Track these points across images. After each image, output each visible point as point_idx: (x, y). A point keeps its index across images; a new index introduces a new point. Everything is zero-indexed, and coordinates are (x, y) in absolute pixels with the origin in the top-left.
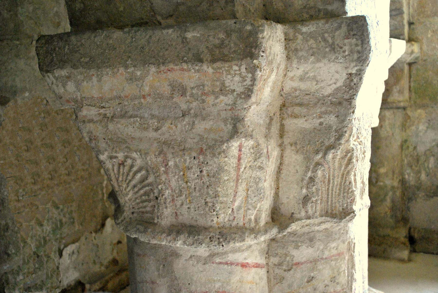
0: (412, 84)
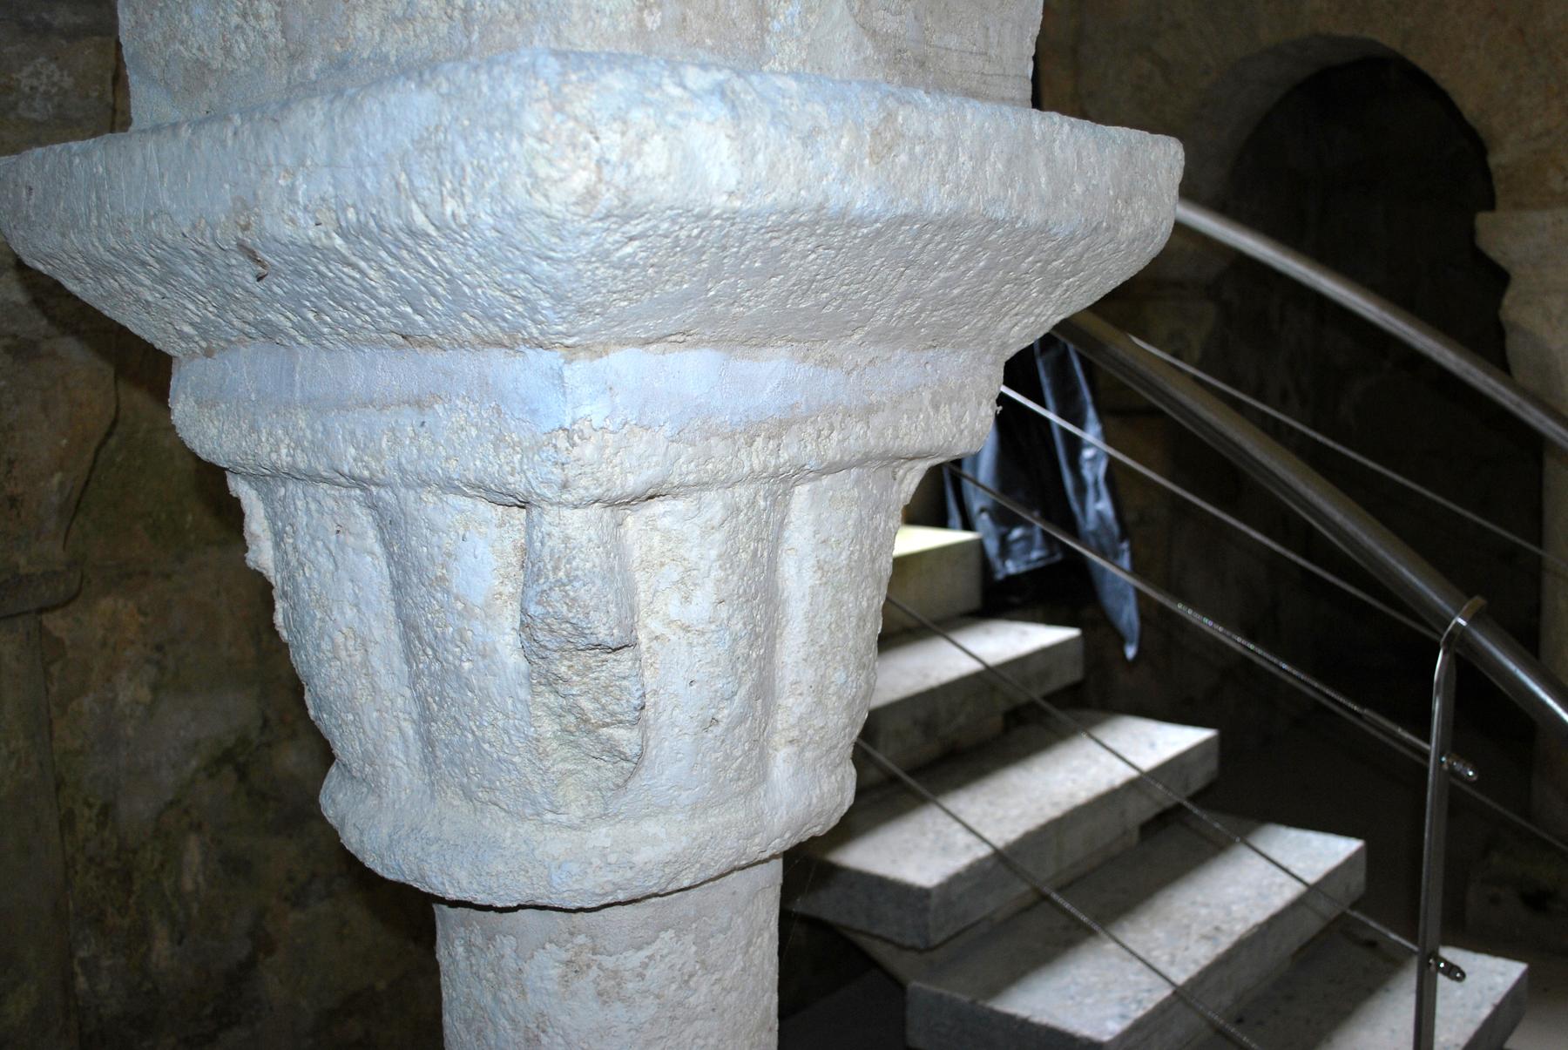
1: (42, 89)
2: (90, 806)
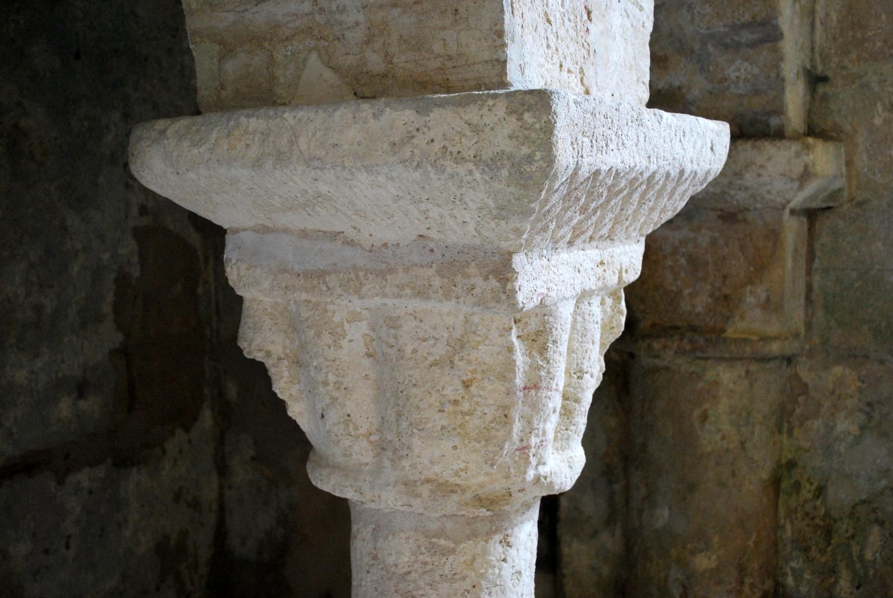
0: (817, 279)
1: (743, 77)
2: (811, 484)
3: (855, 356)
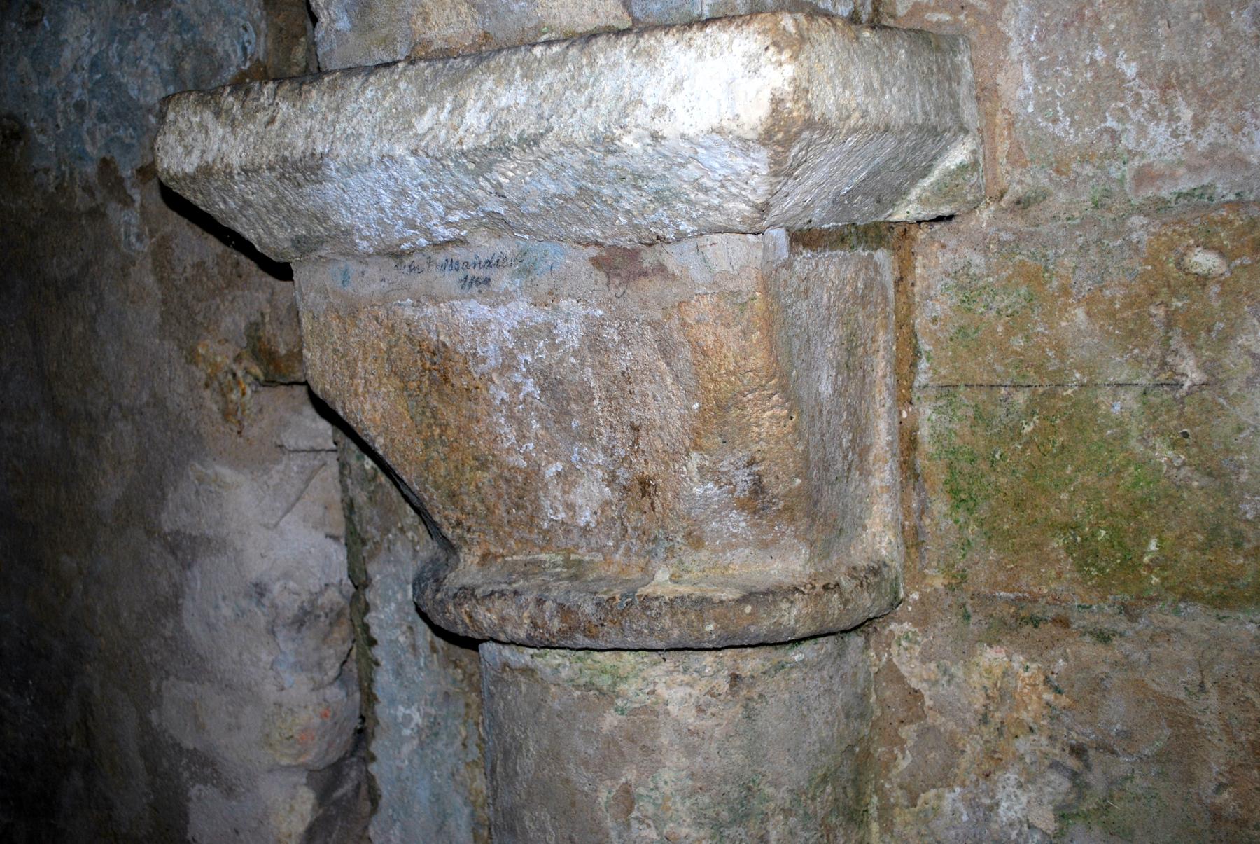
3: (1036, 622)
